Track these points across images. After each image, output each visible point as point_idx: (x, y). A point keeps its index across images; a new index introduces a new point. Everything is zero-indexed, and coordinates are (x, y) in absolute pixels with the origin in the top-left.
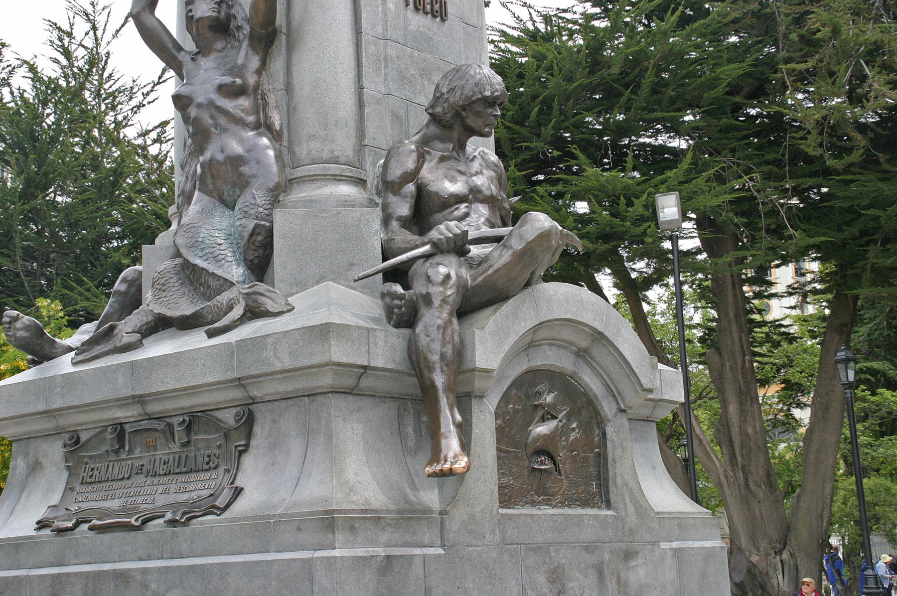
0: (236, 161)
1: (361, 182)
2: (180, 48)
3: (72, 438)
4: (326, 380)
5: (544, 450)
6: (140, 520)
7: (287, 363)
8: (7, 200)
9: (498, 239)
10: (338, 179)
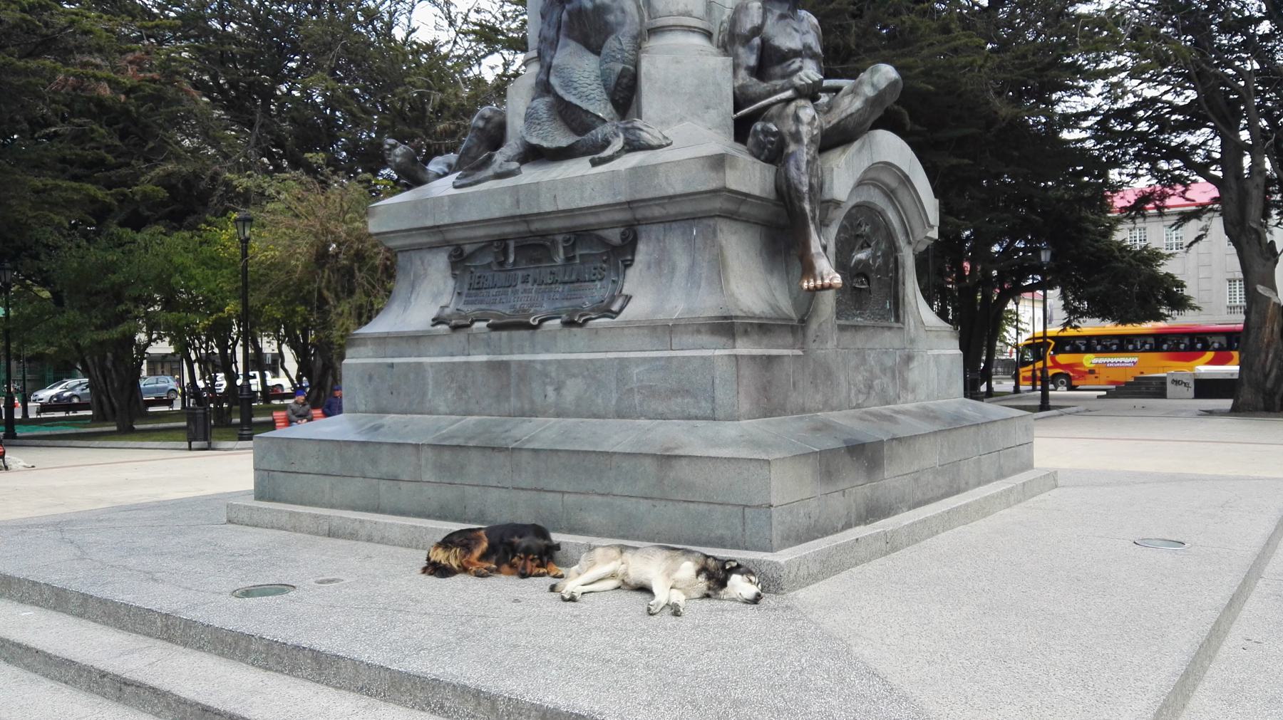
3: (455, 250)
4: (717, 204)
6: (537, 320)
7: (679, 188)
8: (304, 55)
10: (690, 29)
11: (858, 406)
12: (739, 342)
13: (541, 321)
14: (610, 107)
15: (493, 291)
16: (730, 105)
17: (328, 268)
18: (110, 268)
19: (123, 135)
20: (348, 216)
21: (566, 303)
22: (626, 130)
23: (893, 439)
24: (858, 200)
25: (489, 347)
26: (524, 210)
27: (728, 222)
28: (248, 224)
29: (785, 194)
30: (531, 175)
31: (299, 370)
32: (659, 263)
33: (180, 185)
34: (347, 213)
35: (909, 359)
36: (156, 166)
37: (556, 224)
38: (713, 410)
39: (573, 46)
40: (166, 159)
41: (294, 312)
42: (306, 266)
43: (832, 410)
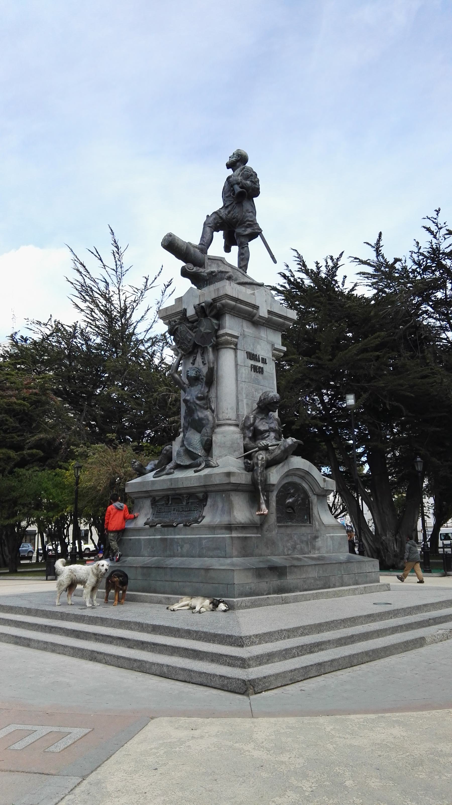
0: (201, 420)
1: (237, 425)
2: (185, 384)
3: (153, 499)
4: (229, 487)
5: (290, 506)
7: (218, 482)
9: (278, 445)
11: (288, 555)
12: (233, 532)
13: (177, 525)
14: (203, 451)
15: (164, 514)
16: (242, 450)
17: (115, 490)
18: (12, 489)
19: (21, 421)
20: (125, 465)
21: (186, 518)
22: (206, 461)
23: (291, 566)
24: (287, 481)
25: (162, 533)
26: (173, 486)
27: (234, 492)
28: (79, 469)
29: (254, 483)
30: (178, 474)
31: (99, 540)
32: (214, 505)
33: (45, 444)
34: (125, 463)
35: (316, 537)
36: (35, 435)
37: (183, 491)
38: (226, 554)
39: (193, 431)
40: (40, 432)
41: (98, 510)
42: (105, 488)
43: (275, 555)
